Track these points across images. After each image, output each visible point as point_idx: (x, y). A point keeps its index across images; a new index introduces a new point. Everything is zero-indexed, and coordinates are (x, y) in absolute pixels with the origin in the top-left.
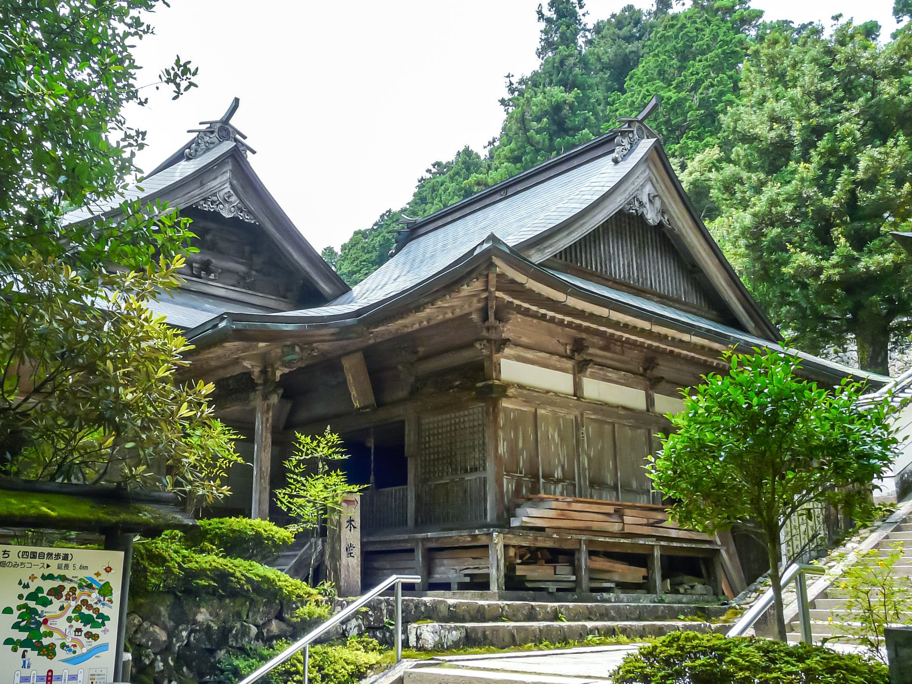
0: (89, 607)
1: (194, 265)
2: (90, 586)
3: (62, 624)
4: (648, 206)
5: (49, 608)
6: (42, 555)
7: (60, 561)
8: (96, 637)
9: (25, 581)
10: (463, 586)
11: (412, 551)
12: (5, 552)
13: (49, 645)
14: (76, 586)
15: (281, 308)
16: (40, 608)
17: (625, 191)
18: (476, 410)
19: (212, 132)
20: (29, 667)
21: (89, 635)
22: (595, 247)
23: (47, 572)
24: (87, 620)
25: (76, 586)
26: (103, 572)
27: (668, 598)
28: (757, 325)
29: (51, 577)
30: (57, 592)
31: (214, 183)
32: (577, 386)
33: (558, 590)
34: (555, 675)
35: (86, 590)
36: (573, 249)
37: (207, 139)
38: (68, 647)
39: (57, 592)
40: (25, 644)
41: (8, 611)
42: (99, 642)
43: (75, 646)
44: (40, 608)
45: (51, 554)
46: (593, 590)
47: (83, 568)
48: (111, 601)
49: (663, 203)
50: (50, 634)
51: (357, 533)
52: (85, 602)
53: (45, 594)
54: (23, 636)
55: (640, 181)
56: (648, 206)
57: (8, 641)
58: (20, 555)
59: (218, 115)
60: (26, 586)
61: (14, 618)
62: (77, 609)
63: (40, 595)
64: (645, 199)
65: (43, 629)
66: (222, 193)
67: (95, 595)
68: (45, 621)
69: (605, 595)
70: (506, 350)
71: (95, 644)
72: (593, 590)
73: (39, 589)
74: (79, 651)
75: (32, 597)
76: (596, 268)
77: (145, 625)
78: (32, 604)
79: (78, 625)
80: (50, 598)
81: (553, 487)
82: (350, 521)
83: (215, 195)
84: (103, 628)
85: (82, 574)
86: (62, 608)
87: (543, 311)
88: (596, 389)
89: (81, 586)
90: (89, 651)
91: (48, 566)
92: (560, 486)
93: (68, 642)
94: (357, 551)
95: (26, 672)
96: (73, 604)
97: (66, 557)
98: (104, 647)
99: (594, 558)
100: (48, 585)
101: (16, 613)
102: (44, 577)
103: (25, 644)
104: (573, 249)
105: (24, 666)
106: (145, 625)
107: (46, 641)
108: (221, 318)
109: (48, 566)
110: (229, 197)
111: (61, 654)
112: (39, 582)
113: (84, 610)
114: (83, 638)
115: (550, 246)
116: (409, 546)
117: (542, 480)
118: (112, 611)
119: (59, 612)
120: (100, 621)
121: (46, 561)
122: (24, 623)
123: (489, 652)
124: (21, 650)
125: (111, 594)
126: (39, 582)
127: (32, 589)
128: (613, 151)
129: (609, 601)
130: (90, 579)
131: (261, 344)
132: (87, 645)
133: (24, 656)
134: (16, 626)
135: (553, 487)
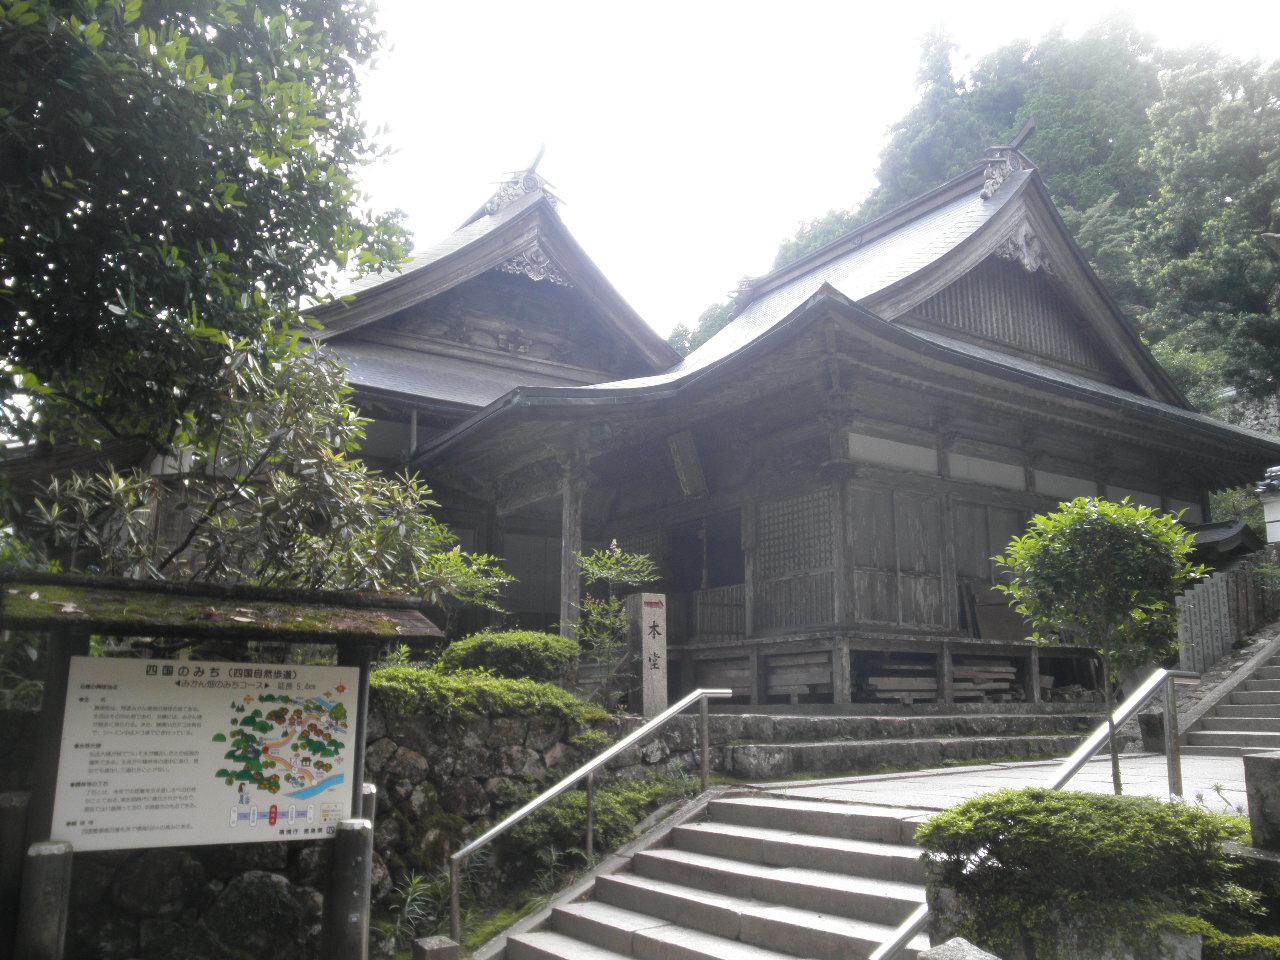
0: (319, 732)
1: (501, 337)
2: (319, 708)
3: (286, 752)
4: (1024, 250)
5: (270, 734)
6: (258, 673)
7: (282, 680)
8: (328, 767)
9: (240, 702)
10: (805, 699)
11: (746, 658)
12: (213, 670)
13: (271, 777)
14: (302, 708)
15: (585, 380)
16: (258, 735)
17: (998, 230)
18: (821, 494)
19: (516, 183)
20: (247, 802)
21: (319, 765)
22: (962, 300)
23: (265, 693)
24: (317, 748)
25: (302, 708)
26: (335, 693)
27: (1049, 707)
28: (1157, 387)
29: (270, 698)
30: (278, 716)
31: (521, 241)
32: (942, 462)
33: (916, 701)
34: (874, 805)
35: (314, 713)
36: (935, 301)
37: (510, 191)
38: (294, 779)
39: (278, 716)
40: (241, 775)
41: (220, 738)
42: (332, 773)
43: (302, 778)
44: (258, 735)
45: (270, 672)
46: (958, 700)
47: (309, 687)
48: (345, 726)
49: (1042, 245)
50: (272, 765)
51: (662, 640)
52: (313, 727)
53: (264, 718)
54: (239, 766)
55: (1015, 219)
56: (1024, 250)
57: (222, 773)
58: (232, 673)
59: (523, 166)
60: (241, 709)
61: (228, 746)
62: (304, 735)
63: (258, 720)
64: (1021, 241)
65: (263, 759)
66: (529, 253)
67: (325, 718)
68: (266, 750)
69: (972, 706)
70: (855, 422)
71: (327, 775)
72: (958, 700)
73: (257, 713)
74: (307, 783)
75: (248, 721)
76: (964, 324)
77: (401, 751)
78: (248, 730)
79: (307, 753)
80: (270, 722)
81: (913, 584)
82: (654, 627)
83: (520, 255)
84: (336, 757)
85: (307, 695)
86: (285, 734)
87: (896, 375)
88: (962, 466)
89: (307, 708)
90: (319, 784)
91: (266, 686)
92: (922, 580)
93: (295, 773)
94: (663, 663)
95: (244, 808)
96: (299, 729)
97: (288, 675)
98: (339, 778)
99: (962, 664)
100: (267, 708)
101: (230, 741)
102: (262, 699)
103: (243, 775)
104: (935, 301)
105: (241, 801)
106: (401, 751)
107: (267, 773)
108: (514, 393)
109: (266, 686)
110: (537, 257)
111: (285, 786)
112: (256, 705)
113: (313, 736)
114: (312, 769)
115: (907, 299)
116: (742, 653)
117: (900, 574)
118: (348, 738)
119: (282, 739)
120: (333, 748)
121: (264, 680)
122: (239, 752)
123: (815, 777)
124: (237, 783)
125: (345, 718)
126: (256, 705)
127: (248, 712)
128: (982, 186)
129: (976, 712)
130: (318, 699)
131: (564, 424)
132: (316, 777)
133: (241, 790)
134: (230, 755)
135: (913, 584)
